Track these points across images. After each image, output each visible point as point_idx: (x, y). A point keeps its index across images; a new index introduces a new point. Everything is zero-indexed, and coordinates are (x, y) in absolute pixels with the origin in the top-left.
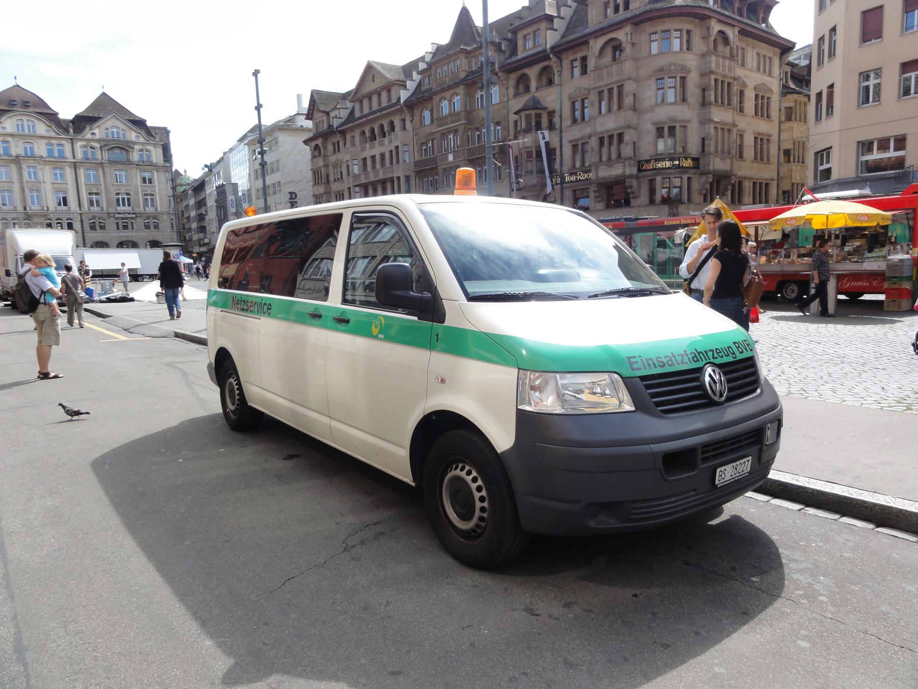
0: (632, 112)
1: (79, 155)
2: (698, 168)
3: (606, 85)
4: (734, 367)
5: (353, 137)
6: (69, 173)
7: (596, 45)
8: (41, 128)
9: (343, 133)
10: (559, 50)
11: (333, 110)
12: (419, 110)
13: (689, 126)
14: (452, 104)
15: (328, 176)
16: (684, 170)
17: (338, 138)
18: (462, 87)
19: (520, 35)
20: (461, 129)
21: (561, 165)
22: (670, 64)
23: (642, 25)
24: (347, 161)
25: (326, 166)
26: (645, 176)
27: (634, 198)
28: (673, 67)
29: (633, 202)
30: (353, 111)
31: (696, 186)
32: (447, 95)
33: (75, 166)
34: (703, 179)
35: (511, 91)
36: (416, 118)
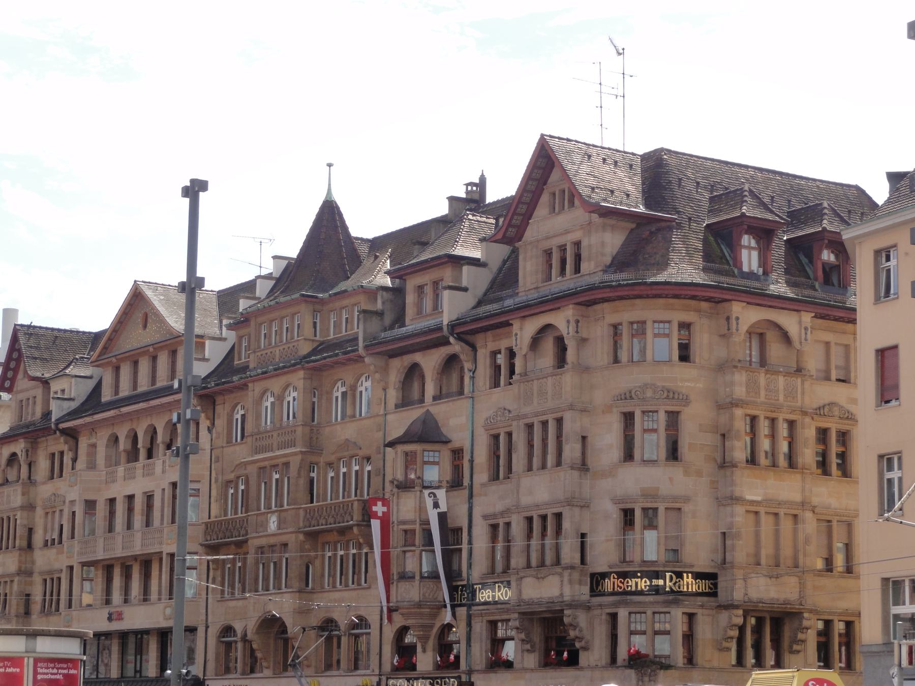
0: (576, 474)
2: (714, 594)
3: (537, 415)
5: (94, 446)
7: (524, 331)
9: (72, 435)
10: (467, 331)
11: (54, 377)
12: (228, 407)
13: (687, 508)
14: (283, 401)
15: (30, 531)
16: (677, 596)
17: (58, 444)
18: (301, 374)
19: (411, 283)
20: (295, 462)
21: (470, 566)
22: (646, 386)
23: (598, 307)
24: (72, 502)
25: (30, 507)
26: (601, 606)
27: (586, 649)
28: (649, 394)
29: (583, 658)
30: (99, 385)
31: (705, 630)
32: (276, 385)
34: (724, 616)
35: (393, 396)
36: (220, 423)
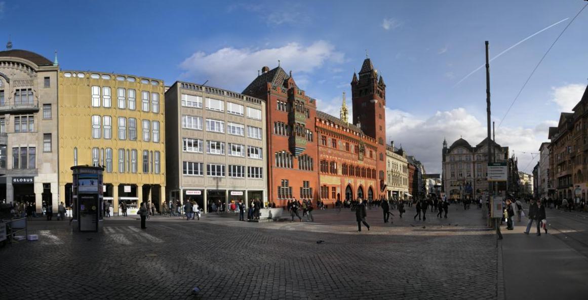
1: (476, 159)
4: (269, 126)
6: (472, 165)
8: (465, 151)
33: (474, 163)
